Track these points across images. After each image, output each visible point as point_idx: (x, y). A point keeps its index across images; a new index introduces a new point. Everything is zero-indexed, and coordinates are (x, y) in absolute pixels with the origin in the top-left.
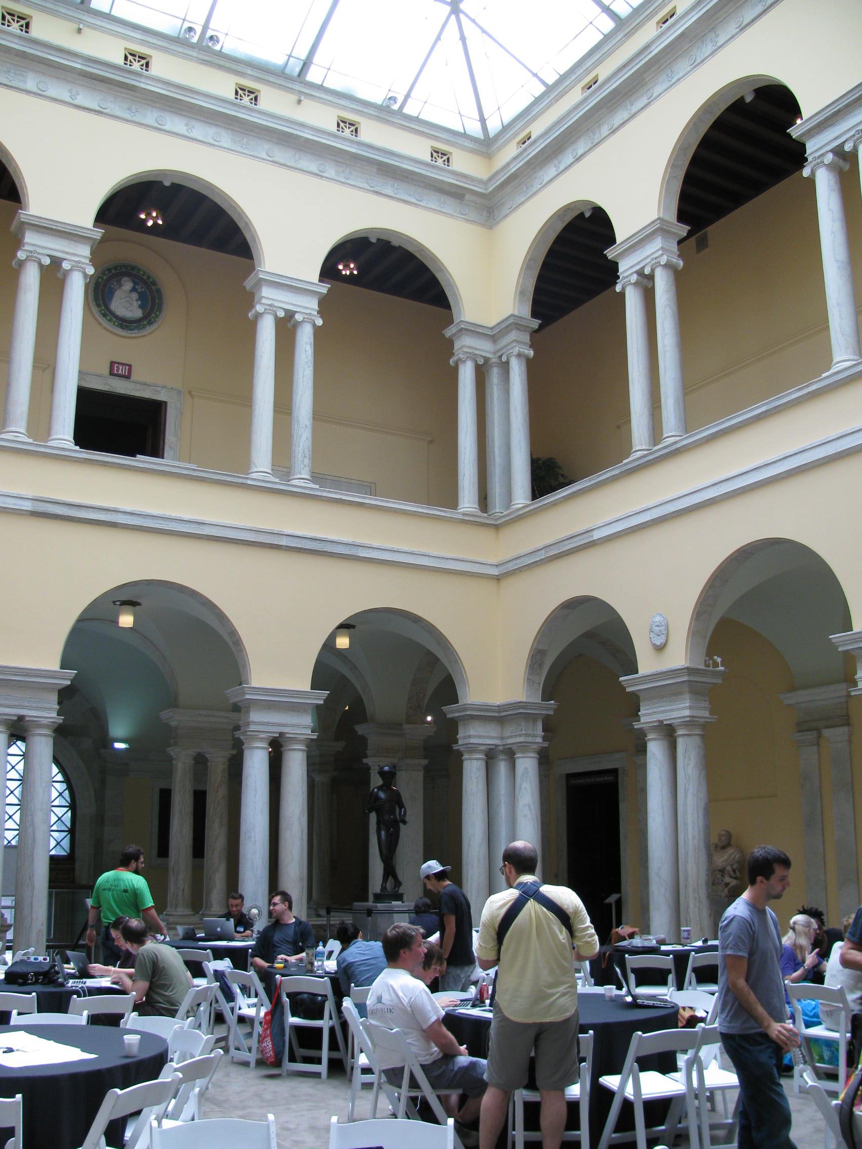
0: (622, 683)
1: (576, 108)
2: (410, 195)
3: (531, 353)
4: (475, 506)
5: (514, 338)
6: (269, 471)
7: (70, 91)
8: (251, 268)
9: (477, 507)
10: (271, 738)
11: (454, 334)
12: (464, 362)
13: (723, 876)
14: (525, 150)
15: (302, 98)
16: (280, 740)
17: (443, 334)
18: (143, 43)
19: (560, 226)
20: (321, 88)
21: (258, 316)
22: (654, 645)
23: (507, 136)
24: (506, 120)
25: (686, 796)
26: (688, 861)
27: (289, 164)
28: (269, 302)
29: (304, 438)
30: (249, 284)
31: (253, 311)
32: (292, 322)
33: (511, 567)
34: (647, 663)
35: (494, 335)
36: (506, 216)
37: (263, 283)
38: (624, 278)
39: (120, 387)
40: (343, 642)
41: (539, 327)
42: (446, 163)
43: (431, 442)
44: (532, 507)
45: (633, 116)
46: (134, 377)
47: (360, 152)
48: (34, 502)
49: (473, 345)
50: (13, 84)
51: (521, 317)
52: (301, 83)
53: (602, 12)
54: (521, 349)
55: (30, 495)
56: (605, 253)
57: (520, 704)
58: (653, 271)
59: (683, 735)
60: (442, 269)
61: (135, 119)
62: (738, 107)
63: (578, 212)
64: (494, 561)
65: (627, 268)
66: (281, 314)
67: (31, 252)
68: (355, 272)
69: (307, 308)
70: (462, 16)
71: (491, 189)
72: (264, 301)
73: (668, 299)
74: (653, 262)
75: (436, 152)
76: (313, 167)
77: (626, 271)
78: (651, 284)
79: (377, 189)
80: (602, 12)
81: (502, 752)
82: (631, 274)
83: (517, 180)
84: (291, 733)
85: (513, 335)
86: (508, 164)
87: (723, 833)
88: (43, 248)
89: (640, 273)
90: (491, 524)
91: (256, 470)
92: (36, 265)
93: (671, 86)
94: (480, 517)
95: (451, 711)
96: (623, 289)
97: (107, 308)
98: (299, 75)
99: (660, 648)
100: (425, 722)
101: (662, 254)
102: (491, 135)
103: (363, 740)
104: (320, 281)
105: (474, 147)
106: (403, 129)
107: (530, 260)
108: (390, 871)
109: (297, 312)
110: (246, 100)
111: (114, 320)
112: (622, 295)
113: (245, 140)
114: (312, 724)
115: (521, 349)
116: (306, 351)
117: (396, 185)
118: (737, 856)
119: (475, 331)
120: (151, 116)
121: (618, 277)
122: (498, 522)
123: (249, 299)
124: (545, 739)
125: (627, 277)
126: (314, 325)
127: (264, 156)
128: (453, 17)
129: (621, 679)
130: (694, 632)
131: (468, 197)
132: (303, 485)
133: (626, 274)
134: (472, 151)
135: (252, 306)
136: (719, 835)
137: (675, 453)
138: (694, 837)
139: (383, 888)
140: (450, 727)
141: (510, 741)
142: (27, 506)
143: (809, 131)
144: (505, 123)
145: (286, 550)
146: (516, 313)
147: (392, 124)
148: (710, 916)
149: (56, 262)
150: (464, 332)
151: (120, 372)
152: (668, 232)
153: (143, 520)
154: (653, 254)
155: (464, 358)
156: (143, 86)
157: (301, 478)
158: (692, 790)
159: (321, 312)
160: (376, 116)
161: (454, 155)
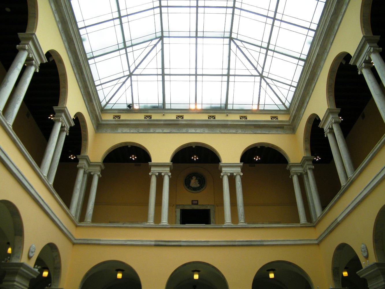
2: (266, 131)
4: (305, 221)
7: (162, 130)
9: (306, 221)
11: (289, 168)
18: (181, 113)
20: (233, 110)
21: (223, 176)
24: (290, 102)
29: (241, 210)
30: (219, 168)
32: (234, 176)
33: (320, 239)
34: (364, 263)
35: (301, 165)
36: (297, 129)
39: (195, 207)
45: (315, 84)
46: (199, 204)
48: (155, 242)
49: (295, 170)
50: (147, 132)
51: (307, 157)
54: (309, 167)
55: (154, 239)
61: (180, 132)
64: (315, 238)
65: (326, 128)
66: (229, 174)
67: (153, 172)
71: (291, 122)
72: (223, 172)
73: (338, 133)
76: (234, 131)
77: (326, 129)
82: (327, 130)
85: (306, 163)
88: (156, 171)
89: (329, 128)
92: (155, 176)
94: (307, 224)
97: (190, 186)
99: (367, 257)
102: (288, 108)
105: (285, 113)
106: (261, 114)
107: (305, 139)
109: (234, 173)
111: (191, 188)
112: (327, 137)
115: (309, 167)
119: (296, 165)
120: (184, 130)
122: (314, 225)
129: (357, 273)
131: (285, 127)
142: (153, 243)
144: (290, 102)
145: (238, 246)
146: (306, 156)
149: (160, 174)
151: (195, 203)
153: (189, 243)
156: (180, 123)
157: (242, 222)
159: (242, 171)
161: (278, 117)
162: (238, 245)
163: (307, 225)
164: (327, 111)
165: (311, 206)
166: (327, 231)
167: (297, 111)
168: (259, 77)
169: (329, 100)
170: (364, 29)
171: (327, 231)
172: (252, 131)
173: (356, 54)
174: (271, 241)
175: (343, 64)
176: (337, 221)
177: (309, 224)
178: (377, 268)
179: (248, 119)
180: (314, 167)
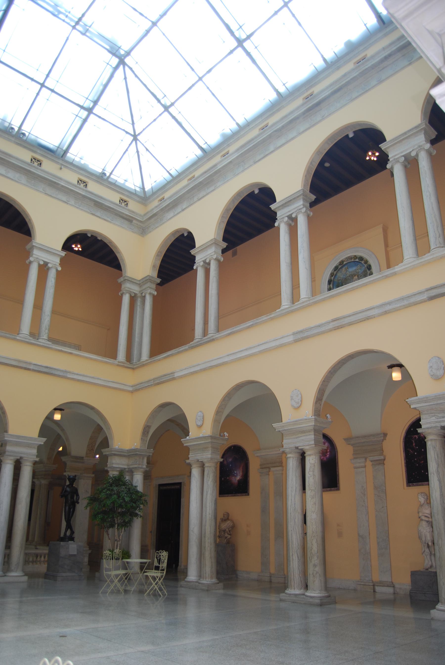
0: (182, 442)
1: (184, 187)
3: (155, 293)
5: (149, 286)
6: (29, 334)
8: (31, 240)
9: (125, 359)
10: (16, 459)
11: (122, 282)
12: (126, 294)
13: (224, 533)
14: (161, 204)
15: (62, 167)
16: (21, 460)
17: (117, 281)
19: (173, 239)
21: (30, 262)
22: (197, 425)
23: (154, 197)
25: (207, 494)
26: (206, 525)
27: (53, 196)
28: (37, 257)
30: (28, 247)
31: (29, 260)
32: (47, 267)
34: (193, 432)
35: (141, 283)
36: (150, 232)
37: (34, 248)
38: (198, 263)
40: (57, 417)
41: (160, 282)
42: (126, 205)
43: (108, 329)
44: (149, 361)
45: (208, 194)
47: (86, 195)
51: (152, 277)
52: (62, 160)
53: (174, 105)
54: (151, 291)
56: (190, 251)
57: (137, 450)
58: (210, 261)
59: (207, 467)
60: (119, 252)
62: (251, 195)
63: (181, 233)
65: (199, 259)
66: (42, 263)
68: (80, 249)
69: (54, 262)
70: (138, 142)
71: (145, 219)
72: (34, 256)
74: (210, 257)
75: (122, 200)
76: (64, 199)
78: (209, 267)
79: (93, 212)
80: (174, 105)
81: (128, 471)
82: (201, 262)
83: (156, 217)
84: (26, 458)
85: (149, 284)
86: (153, 209)
87: (226, 513)
90: (131, 368)
91: (22, 333)
93: (224, 183)
95: (105, 451)
96: (197, 268)
98: (62, 157)
99: (200, 427)
100: (95, 457)
101: (214, 254)
103: (65, 464)
104: (62, 250)
106: (108, 188)
107: (159, 252)
108: (69, 526)
110: (36, 164)
113: (33, 181)
114: (37, 454)
115: (151, 291)
116: (52, 281)
117: (102, 212)
118: (231, 524)
119: (132, 281)
121: (195, 263)
122: (134, 367)
123: (28, 254)
124: (147, 467)
125: (199, 263)
126: (57, 270)
127: (41, 190)
128: (134, 142)
129: (182, 440)
130: (216, 421)
131: (134, 221)
132: (44, 342)
133: (198, 262)
134: (139, 202)
135: (28, 258)
136: (223, 514)
137: (212, 340)
138: (209, 514)
139: (65, 534)
140: (104, 459)
141: (131, 467)
143: (279, 207)
146: (150, 275)
147: (103, 185)
148: (215, 551)
150: (126, 281)
152: (218, 245)
154: (210, 254)
155: (125, 292)
158: (210, 492)
160: (96, 180)
162: (33, 369)
163: (125, 365)
164: (212, 240)
165: (136, 341)
166: (154, 381)
167: (162, 210)
168: (132, 138)
169: (219, 227)
170: (305, 179)
171: (152, 381)
172: (89, 209)
173: (284, 202)
174: (77, 374)
175: (254, 193)
176: (174, 375)
177: (128, 364)
178: (210, 441)
179: (90, 188)
180: (157, 294)
